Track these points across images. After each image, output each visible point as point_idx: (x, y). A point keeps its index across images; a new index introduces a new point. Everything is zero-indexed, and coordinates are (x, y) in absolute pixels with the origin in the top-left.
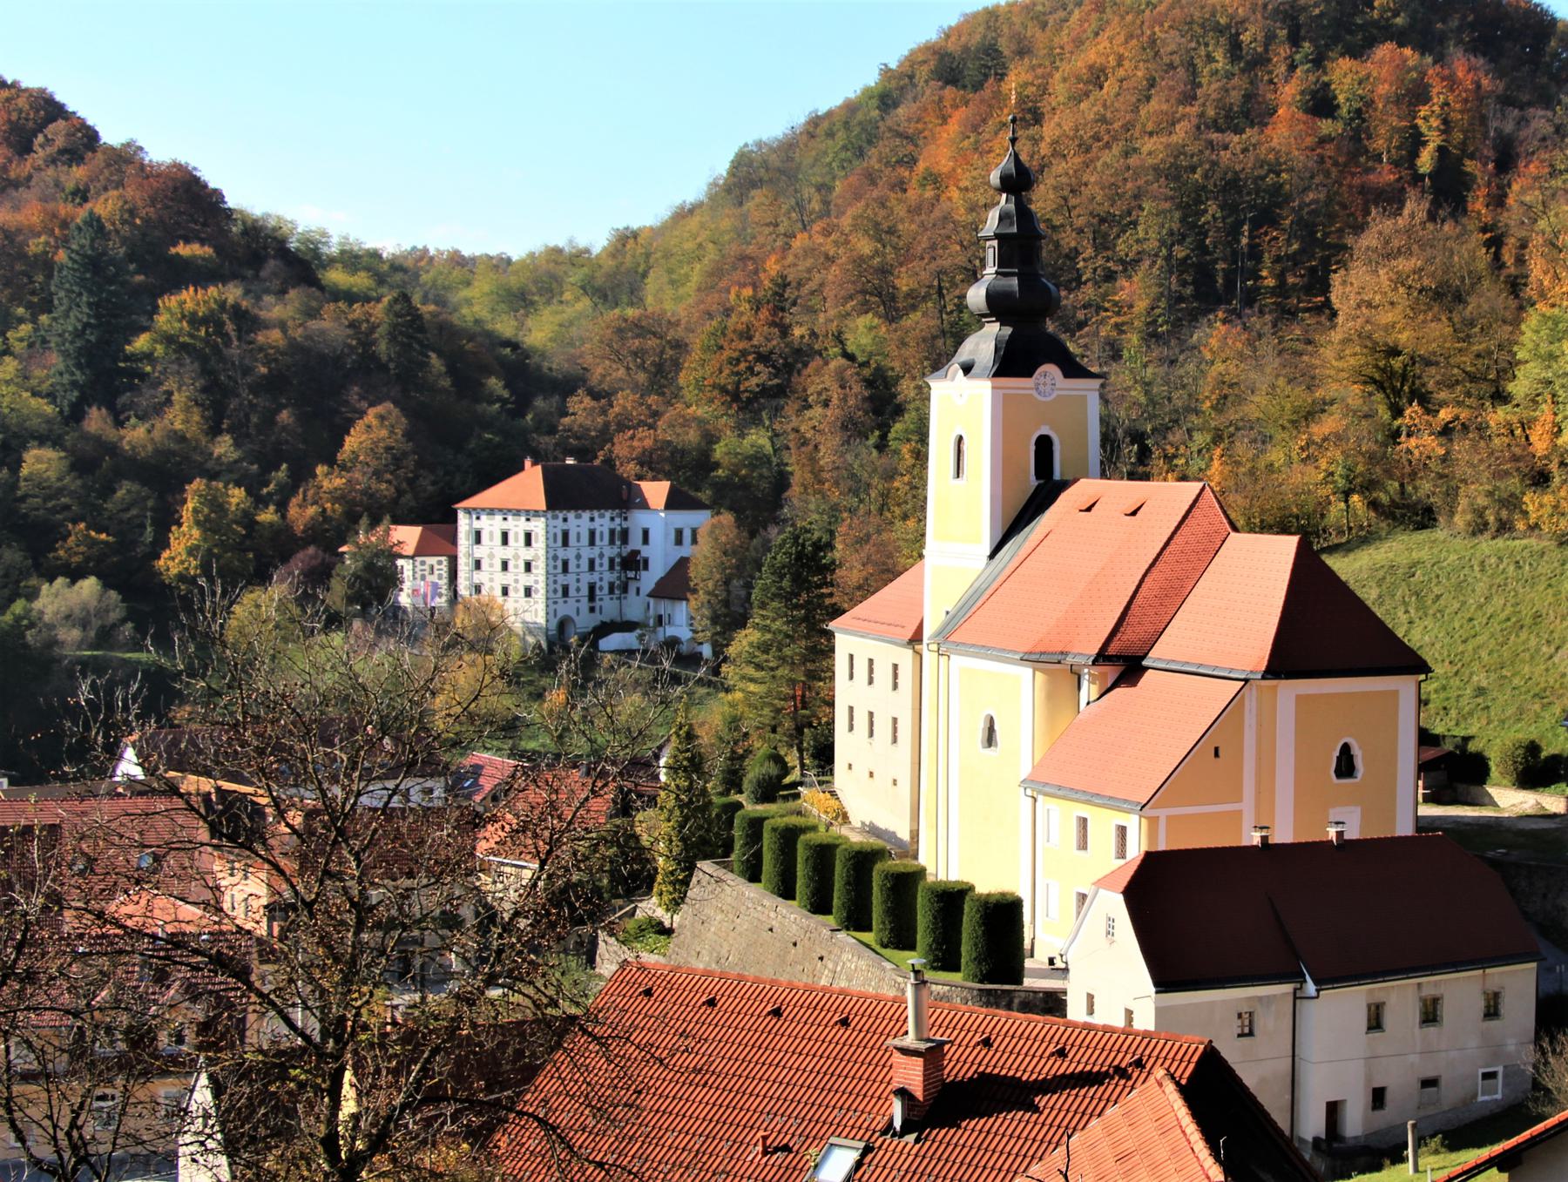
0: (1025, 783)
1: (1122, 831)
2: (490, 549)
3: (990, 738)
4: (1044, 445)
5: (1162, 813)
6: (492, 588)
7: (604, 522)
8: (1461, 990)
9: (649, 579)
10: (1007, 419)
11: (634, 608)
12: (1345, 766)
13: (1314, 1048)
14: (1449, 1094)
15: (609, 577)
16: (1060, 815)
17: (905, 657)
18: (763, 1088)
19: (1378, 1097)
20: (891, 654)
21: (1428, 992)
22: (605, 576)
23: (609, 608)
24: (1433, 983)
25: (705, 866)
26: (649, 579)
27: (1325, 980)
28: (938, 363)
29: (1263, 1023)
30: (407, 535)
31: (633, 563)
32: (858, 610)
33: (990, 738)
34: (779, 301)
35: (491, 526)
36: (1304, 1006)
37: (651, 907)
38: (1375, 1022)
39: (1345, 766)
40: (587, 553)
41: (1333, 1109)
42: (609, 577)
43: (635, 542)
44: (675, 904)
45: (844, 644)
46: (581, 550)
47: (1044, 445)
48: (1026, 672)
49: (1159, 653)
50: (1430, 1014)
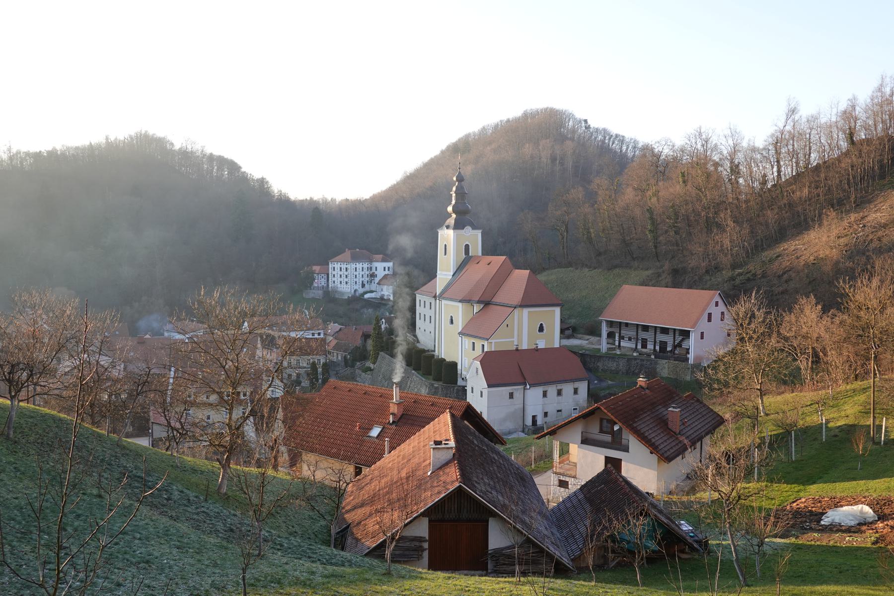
0: (459, 333)
1: (483, 346)
2: (337, 271)
3: (452, 322)
4: (467, 247)
5: (493, 341)
6: (337, 283)
7: (366, 265)
8: (568, 388)
9: (377, 280)
10: (457, 239)
11: (374, 287)
12: (541, 329)
13: (529, 401)
14: (564, 414)
15: (367, 279)
16: (468, 342)
17: (433, 301)
18: (344, 413)
19: (546, 414)
20: (429, 300)
21: (559, 388)
22: (366, 279)
23: (367, 287)
24: (545, 388)
25: (382, 353)
26: (377, 280)
27: (532, 385)
28: (440, 225)
29: (515, 395)
30: (316, 268)
31: (373, 276)
32: (424, 288)
33: (452, 322)
34: (819, 114)
35: (337, 266)
36: (528, 392)
37: (369, 364)
38: (545, 394)
39: (541, 329)
40: (361, 273)
41: (534, 417)
42: (367, 279)
43: (374, 270)
44: (374, 363)
45: (418, 297)
46: (359, 272)
47: (467, 247)
48: (460, 305)
49: (496, 299)
50: (559, 393)
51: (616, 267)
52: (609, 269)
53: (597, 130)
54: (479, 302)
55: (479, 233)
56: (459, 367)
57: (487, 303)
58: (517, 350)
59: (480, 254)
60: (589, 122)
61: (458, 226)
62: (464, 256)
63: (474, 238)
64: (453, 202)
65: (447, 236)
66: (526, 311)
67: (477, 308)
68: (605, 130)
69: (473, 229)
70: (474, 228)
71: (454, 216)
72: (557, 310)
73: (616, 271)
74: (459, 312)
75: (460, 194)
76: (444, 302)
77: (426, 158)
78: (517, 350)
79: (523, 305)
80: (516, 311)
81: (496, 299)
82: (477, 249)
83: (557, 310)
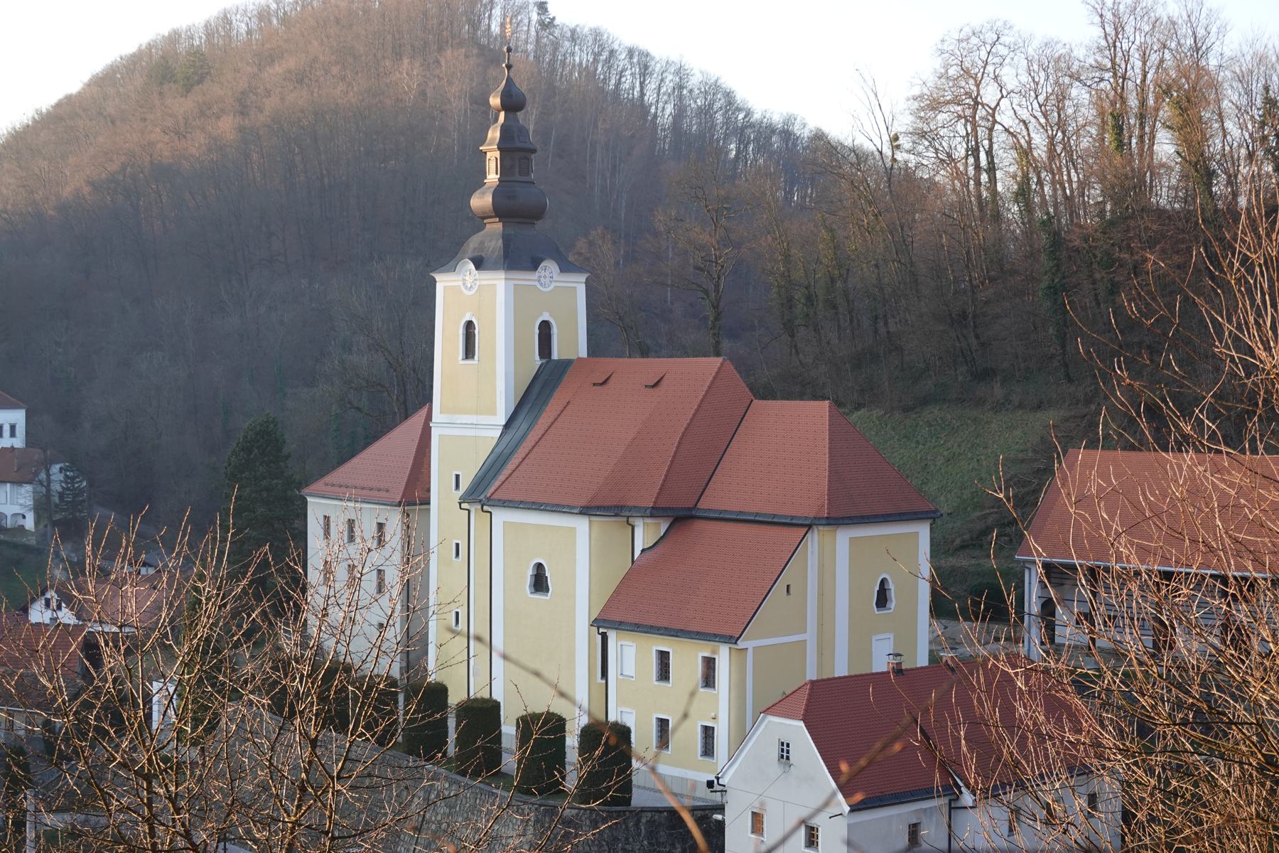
4: (545, 328)
47: (545, 328)
48: (581, 526)
51: (925, 401)
52: (907, 410)
53: (574, 36)
54: (655, 512)
55: (577, 285)
56: (633, 736)
57: (681, 518)
58: (898, 671)
59: (583, 353)
60: (553, 10)
61: (517, 257)
62: (537, 361)
63: (564, 296)
64: (492, 177)
65: (473, 299)
66: (843, 538)
67: (644, 534)
68: (597, 35)
69: (563, 270)
70: (566, 267)
71: (495, 227)
72: (923, 532)
73: (933, 413)
74: (581, 552)
75: (513, 148)
76: (501, 517)
77: (46, 99)
78: (898, 671)
79: (835, 521)
80: (814, 540)
81: (717, 498)
82: (573, 341)
83: (923, 532)
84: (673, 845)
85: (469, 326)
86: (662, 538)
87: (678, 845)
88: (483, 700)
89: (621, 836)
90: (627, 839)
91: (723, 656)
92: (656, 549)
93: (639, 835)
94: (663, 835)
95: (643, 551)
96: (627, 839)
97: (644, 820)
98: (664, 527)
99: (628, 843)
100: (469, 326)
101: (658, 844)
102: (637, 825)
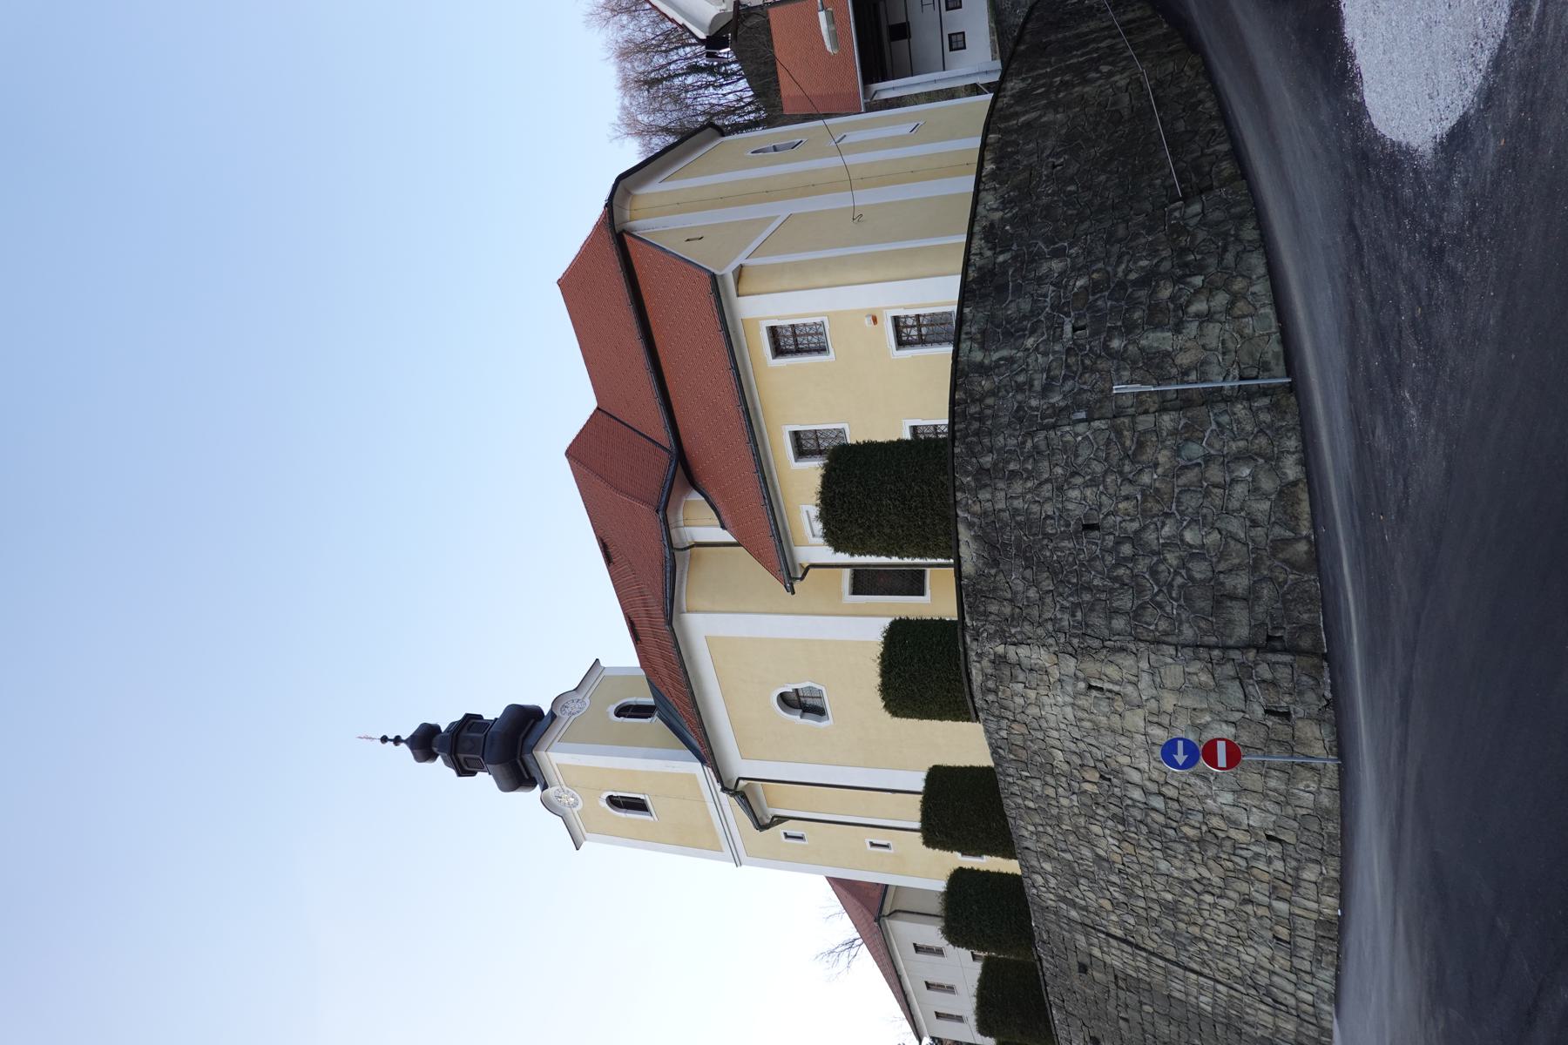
4: (623, 711)
47: (623, 711)
54: (663, 508)
62: (655, 720)
84: (1040, 281)
85: (614, 802)
86: (707, 499)
87: (1044, 269)
88: (925, 803)
89: (1011, 401)
90: (1019, 388)
91: (759, 310)
92: (720, 509)
93: (1011, 360)
94: (1017, 306)
95: (723, 527)
96: (1019, 388)
97: (978, 356)
98: (696, 497)
99: (1030, 383)
100: (614, 802)
101: (1035, 312)
102: (983, 370)
